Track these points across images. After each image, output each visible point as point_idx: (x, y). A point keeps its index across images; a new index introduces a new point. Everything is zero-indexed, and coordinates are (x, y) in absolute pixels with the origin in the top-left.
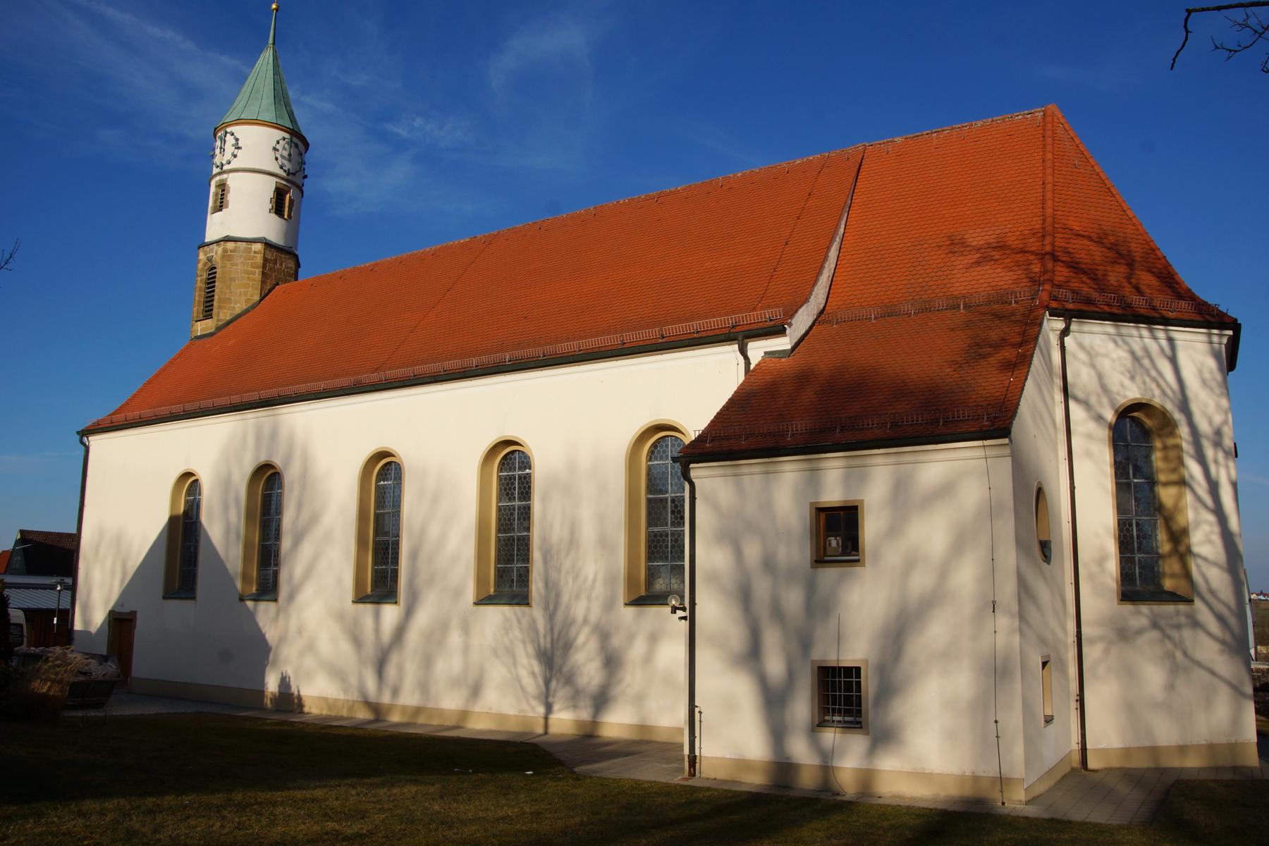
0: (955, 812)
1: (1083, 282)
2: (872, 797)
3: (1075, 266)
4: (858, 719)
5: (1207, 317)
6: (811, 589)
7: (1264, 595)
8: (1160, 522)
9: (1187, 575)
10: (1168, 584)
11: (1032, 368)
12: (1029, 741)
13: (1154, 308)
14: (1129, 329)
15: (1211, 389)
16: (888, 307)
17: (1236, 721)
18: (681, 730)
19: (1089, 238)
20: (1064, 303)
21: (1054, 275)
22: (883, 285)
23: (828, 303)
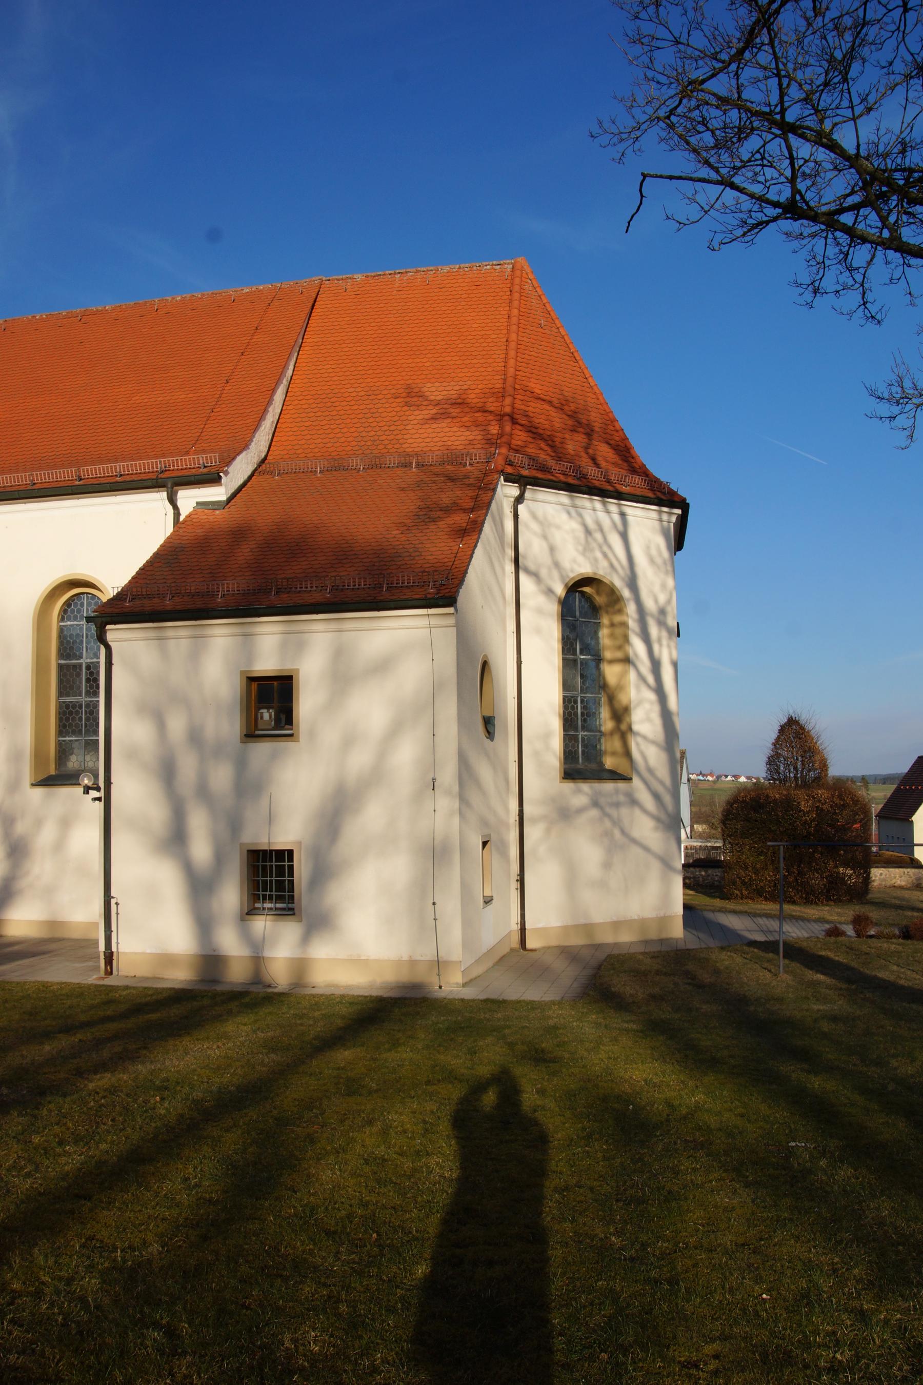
0: (391, 998)
1: (541, 449)
2: (306, 987)
3: (534, 432)
4: (290, 906)
5: (659, 494)
6: (241, 765)
7: (703, 776)
8: (604, 700)
9: (628, 754)
10: (609, 762)
11: (482, 536)
12: (467, 923)
13: (609, 482)
14: (584, 501)
15: (659, 568)
16: (335, 460)
17: (666, 897)
18: (96, 925)
19: (550, 403)
20: (520, 469)
21: (512, 439)
22: (331, 436)
23: (270, 453)
